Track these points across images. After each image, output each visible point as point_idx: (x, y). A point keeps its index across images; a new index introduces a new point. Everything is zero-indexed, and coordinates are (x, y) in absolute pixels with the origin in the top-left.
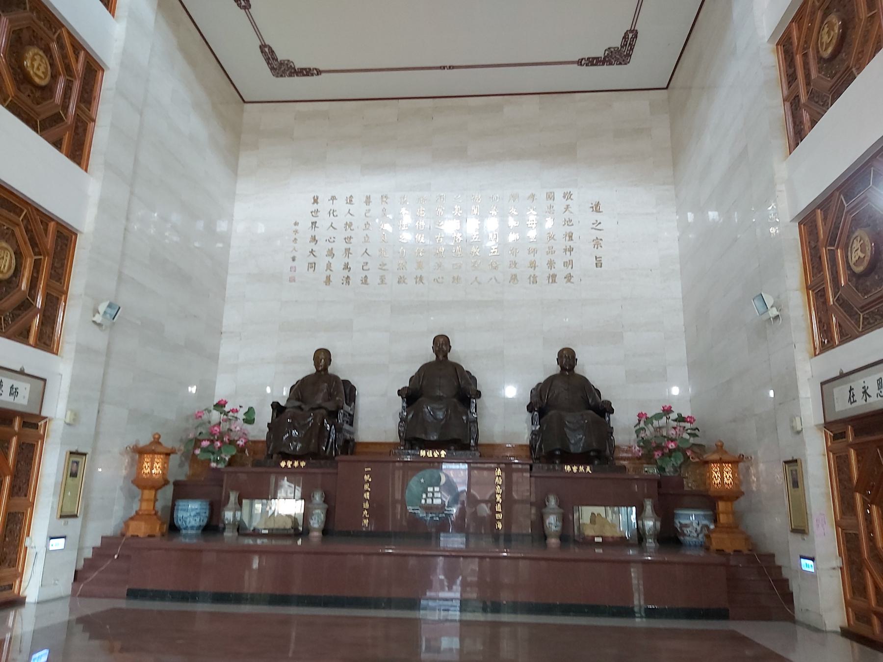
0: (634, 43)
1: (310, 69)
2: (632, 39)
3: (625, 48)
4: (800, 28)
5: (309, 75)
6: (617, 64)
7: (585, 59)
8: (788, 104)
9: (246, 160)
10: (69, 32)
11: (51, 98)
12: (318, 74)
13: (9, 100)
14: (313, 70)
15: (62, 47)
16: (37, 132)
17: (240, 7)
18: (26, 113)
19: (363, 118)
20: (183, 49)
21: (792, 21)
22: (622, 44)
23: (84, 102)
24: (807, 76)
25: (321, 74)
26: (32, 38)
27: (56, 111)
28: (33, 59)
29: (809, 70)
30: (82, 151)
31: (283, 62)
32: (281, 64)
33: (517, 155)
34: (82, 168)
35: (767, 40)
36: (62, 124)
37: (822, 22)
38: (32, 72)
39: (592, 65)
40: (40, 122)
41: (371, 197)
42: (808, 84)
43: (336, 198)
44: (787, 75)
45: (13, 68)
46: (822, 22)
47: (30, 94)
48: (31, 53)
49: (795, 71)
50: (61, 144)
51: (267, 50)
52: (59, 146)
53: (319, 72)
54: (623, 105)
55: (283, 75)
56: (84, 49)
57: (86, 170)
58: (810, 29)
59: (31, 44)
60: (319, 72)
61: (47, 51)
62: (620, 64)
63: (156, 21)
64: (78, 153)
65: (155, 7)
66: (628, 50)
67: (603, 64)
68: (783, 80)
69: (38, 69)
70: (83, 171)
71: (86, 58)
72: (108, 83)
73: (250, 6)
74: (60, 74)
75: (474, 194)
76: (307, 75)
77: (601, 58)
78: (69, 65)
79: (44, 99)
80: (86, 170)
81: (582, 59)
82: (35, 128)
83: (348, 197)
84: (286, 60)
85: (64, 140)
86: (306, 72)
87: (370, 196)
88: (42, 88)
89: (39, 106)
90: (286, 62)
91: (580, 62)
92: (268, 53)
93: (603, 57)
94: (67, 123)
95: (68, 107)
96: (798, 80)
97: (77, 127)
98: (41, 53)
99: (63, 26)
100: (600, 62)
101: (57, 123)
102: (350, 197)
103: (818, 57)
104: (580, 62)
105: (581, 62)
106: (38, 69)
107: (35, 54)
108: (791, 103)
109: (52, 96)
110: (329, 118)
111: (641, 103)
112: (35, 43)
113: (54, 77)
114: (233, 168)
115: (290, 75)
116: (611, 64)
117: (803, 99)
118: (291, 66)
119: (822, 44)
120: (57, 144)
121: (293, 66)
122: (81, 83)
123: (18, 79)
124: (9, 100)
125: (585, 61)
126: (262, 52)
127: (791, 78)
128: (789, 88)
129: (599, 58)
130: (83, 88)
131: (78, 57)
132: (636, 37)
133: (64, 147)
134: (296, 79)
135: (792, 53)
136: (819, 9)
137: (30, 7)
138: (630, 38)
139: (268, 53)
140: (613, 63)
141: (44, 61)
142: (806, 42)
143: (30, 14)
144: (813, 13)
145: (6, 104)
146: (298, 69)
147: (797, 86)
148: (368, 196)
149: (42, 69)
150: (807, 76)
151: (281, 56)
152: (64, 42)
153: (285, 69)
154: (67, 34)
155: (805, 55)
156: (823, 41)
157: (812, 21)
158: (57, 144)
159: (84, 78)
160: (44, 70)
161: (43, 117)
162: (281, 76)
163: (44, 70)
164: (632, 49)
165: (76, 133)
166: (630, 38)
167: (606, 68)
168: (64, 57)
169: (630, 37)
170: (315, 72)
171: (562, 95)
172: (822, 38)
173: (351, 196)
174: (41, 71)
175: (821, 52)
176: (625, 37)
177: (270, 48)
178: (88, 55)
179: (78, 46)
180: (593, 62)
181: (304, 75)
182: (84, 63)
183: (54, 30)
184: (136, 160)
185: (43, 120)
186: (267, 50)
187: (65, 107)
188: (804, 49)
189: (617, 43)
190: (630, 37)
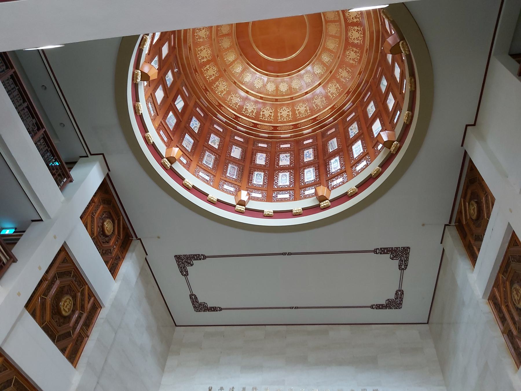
0: (402, 297)
1: (216, 307)
2: (401, 295)
3: (397, 299)
4: (499, 291)
5: (215, 311)
6: (394, 309)
7: (375, 305)
8: (505, 335)
9: (171, 362)
10: (89, 287)
11: (68, 323)
12: (220, 310)
13: (45, 323)
14: (218, 308)
15: (83, 294)
16: (54, 342)
17: (183, 275)
18: (51, 331)
19: (244, 336)
20: (148, 297)
21: (493, 287)
22: (396, 298)
23: (86, 326)
24: (513, 318)
25: (222, 310)
26: (69, 291)
27: (68, 330)
28: (66, 301)
29: (512, 315)
30: (76, 355)
31: (201, 303)
32: (200, 304)
33: (340, 363)
34: (73, 366)
35: (481, 297)
36: (70, 338)
37: (511, 288)
38: (62, 308)
39: (380, 308)
40: (58, 336)
41: (246, 388)
42: (515, 323)
43: (224, 388)
44: (500, 317)
45: (53, 306)
46: (511, 288)
47: (58, 321)
48: (65, 298)
49: (504, 315)
50: (65, 351)
51: (184, 273)
52: (64, 351)
53: (221, 309)
54: (401, 332)
55: (201, 311)
56: (94, 296)
57: (75, 367)
58: (505, 292)
59: (67, 294)
60: (221, 309)
61: (74, 297)
62: (396, 308)
63: (137, 282)
64: (73, 356)
65: (138, 274)
66: (399, 301)
67: (386, 309)
68: (499, 323)
69: (66, 307)
70: (73, 368)
71: (94, 300)
72: (102, 314)
73: (188, 274)
74: (77, 310)
75: (313, 389)
76: (214, 311)
77: (384, 305)
78: (83, 305)
79: (64, 323)
80: (75, 367)
81: (373, 305)
82: (53, 340)
83: (231, 388)
84: (203, 303)
85: (67, 348)
86: (214, 309)
87: (245, 388)
88: (65, 317)
89: (60, 327)
90: (203, 304)
91: (372, 307)
92: (193, 298)
93: (385, 304)
94: (72, 338)
95: (76, 328)
96: (508, 321)
97: (77, 341)
98: (71, 298)
99: (87, 284)
100: (384, 307)
101: (67, 338)
102: (232, 388)
103: (515, 308)
104: (372, 307)
105: (373, 307)
106: (66, 307)
107: (68, 299)
108: (507, 335)
109: (69, 322)
110: (224, 336)
111: (414, 332)
112: (69, 293)
113: (73, 312)
114: (162, 367)
115: (204, 311)
116: (391, 308)
117: (515, 332)
118: (206, 306)
119: (515, 300)
120: (63, 350)
121: (207, 306)
122: (87, 315)
123: (54, 312)
124: (45, 323)
125: (375, 306)
126: (190, 298)
127: (503, 319)
128: (503, 326)
129: (383, 305)
130: (87, 317)
131: (90, 300)
132: (403, 294)
133: (67, 352)
134: (207, 313)
135: (499, 305)
136: (507, 281)
137: (73, 275)
138: (400, 294)
139: (193, 298)
140: (392, 308)
141: (71, 302)
142: (505, 298)
143: (72, 278)
144: (504, 283)
145: (43, 326)
146: (209, 307)
147: (508, 324)
148: (244, 388)
149: (68, 307)
150: (513, 318)
151: (201, 300)
152: (84, 293)
153: (202, 307)
154: (88, 288)
155: (507, 306)
156: (515, 298)
157: (505, 287)
158: (63, 351)
159: (90, 312)
160: (69, 308)
161: (60, 333)
162: (199, 311)
163: (69, 308)
164: (402, 300)
165: (76, 344)
166: (400, 294)
167: (388, 311)
168: (83, 300)
169: (403, 266)
170: (202, 257)
171: (363, 325)
172: (514, 297)
173: (233, 388)
174: (67, 308)
175: (516, 305)
176: (397, 293)
177: (195, 296)
178: (95, 298)
179: (91, 294)
180: (379, 307)
181: (212, 311)
182: (93, 303)
183: (81, 286)
184: (106, 361)
185: (60, 336)
186: (184, 273)
187: (74, 328)
188: (505, 302)
189: (392, 296)
190: (403, 266)
